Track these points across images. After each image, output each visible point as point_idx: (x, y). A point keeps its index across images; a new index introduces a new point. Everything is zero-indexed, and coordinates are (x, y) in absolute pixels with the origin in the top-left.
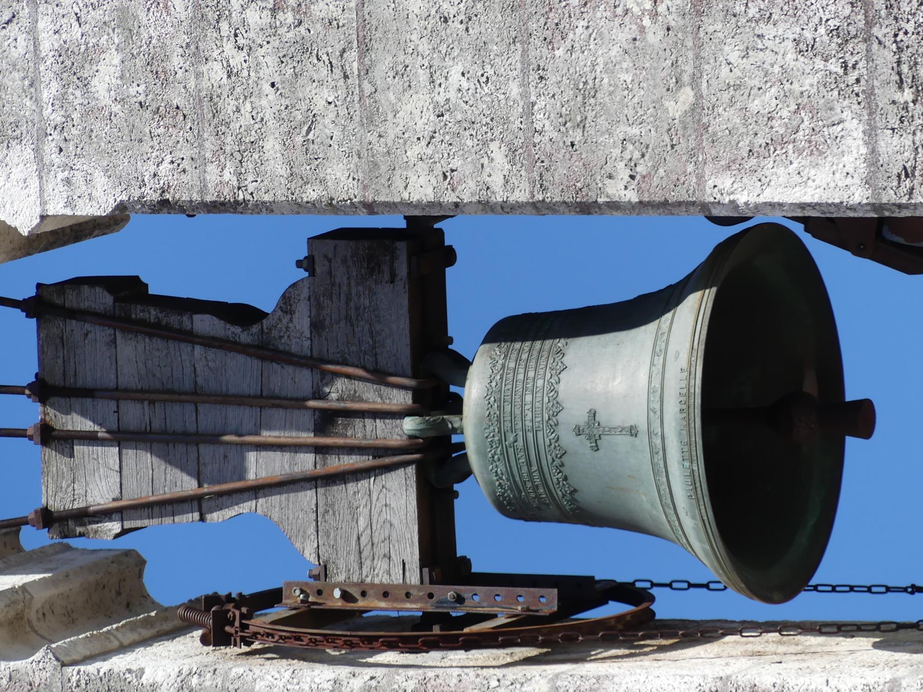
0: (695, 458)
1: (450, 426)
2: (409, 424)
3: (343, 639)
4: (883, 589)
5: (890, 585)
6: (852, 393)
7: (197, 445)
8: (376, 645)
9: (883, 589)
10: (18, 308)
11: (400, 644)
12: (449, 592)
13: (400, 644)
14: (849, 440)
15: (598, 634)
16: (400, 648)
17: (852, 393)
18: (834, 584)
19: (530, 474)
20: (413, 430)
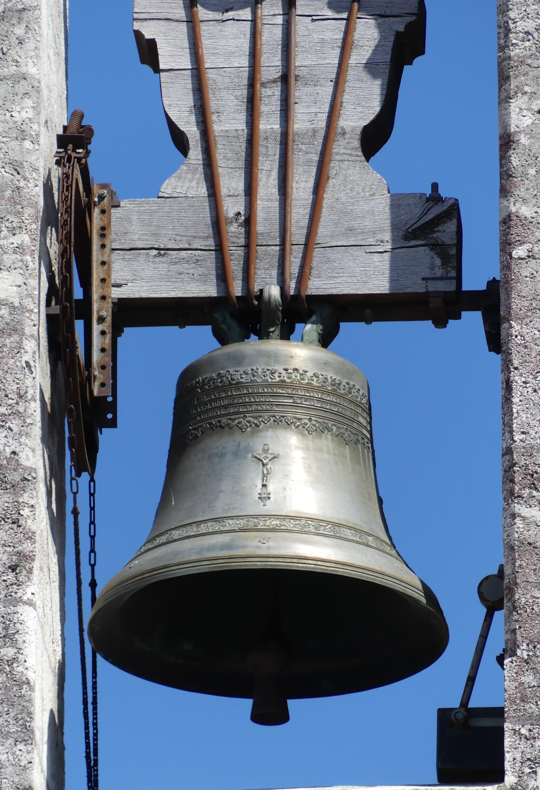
0: (169, 11)
1: (272, 329)
2: (275, 292)
3: (69, 219)
4: (92, 554)
5: (89, 549)
6: (293, 705)
7: (251, 21)
8: (65, 242)
9: (92, 554)
10: (432, 192)
11: (65, 260)
12: (107, 313)
13: (65, 260)
14: (249, 703)
15: (138, 563)
16: (62, 260)
17: (293, 705)
18: (89, 509)
19: (213, 409)
20: (269, 298)
